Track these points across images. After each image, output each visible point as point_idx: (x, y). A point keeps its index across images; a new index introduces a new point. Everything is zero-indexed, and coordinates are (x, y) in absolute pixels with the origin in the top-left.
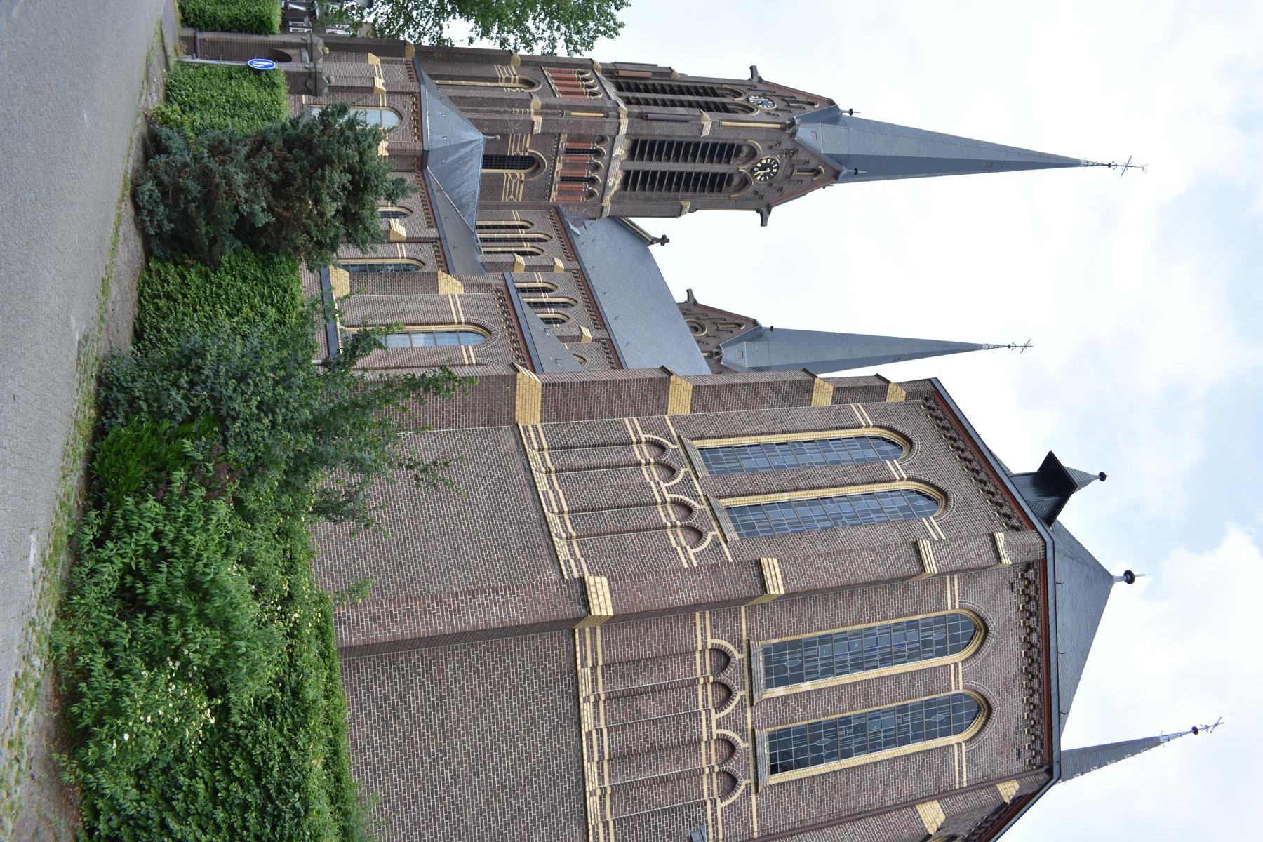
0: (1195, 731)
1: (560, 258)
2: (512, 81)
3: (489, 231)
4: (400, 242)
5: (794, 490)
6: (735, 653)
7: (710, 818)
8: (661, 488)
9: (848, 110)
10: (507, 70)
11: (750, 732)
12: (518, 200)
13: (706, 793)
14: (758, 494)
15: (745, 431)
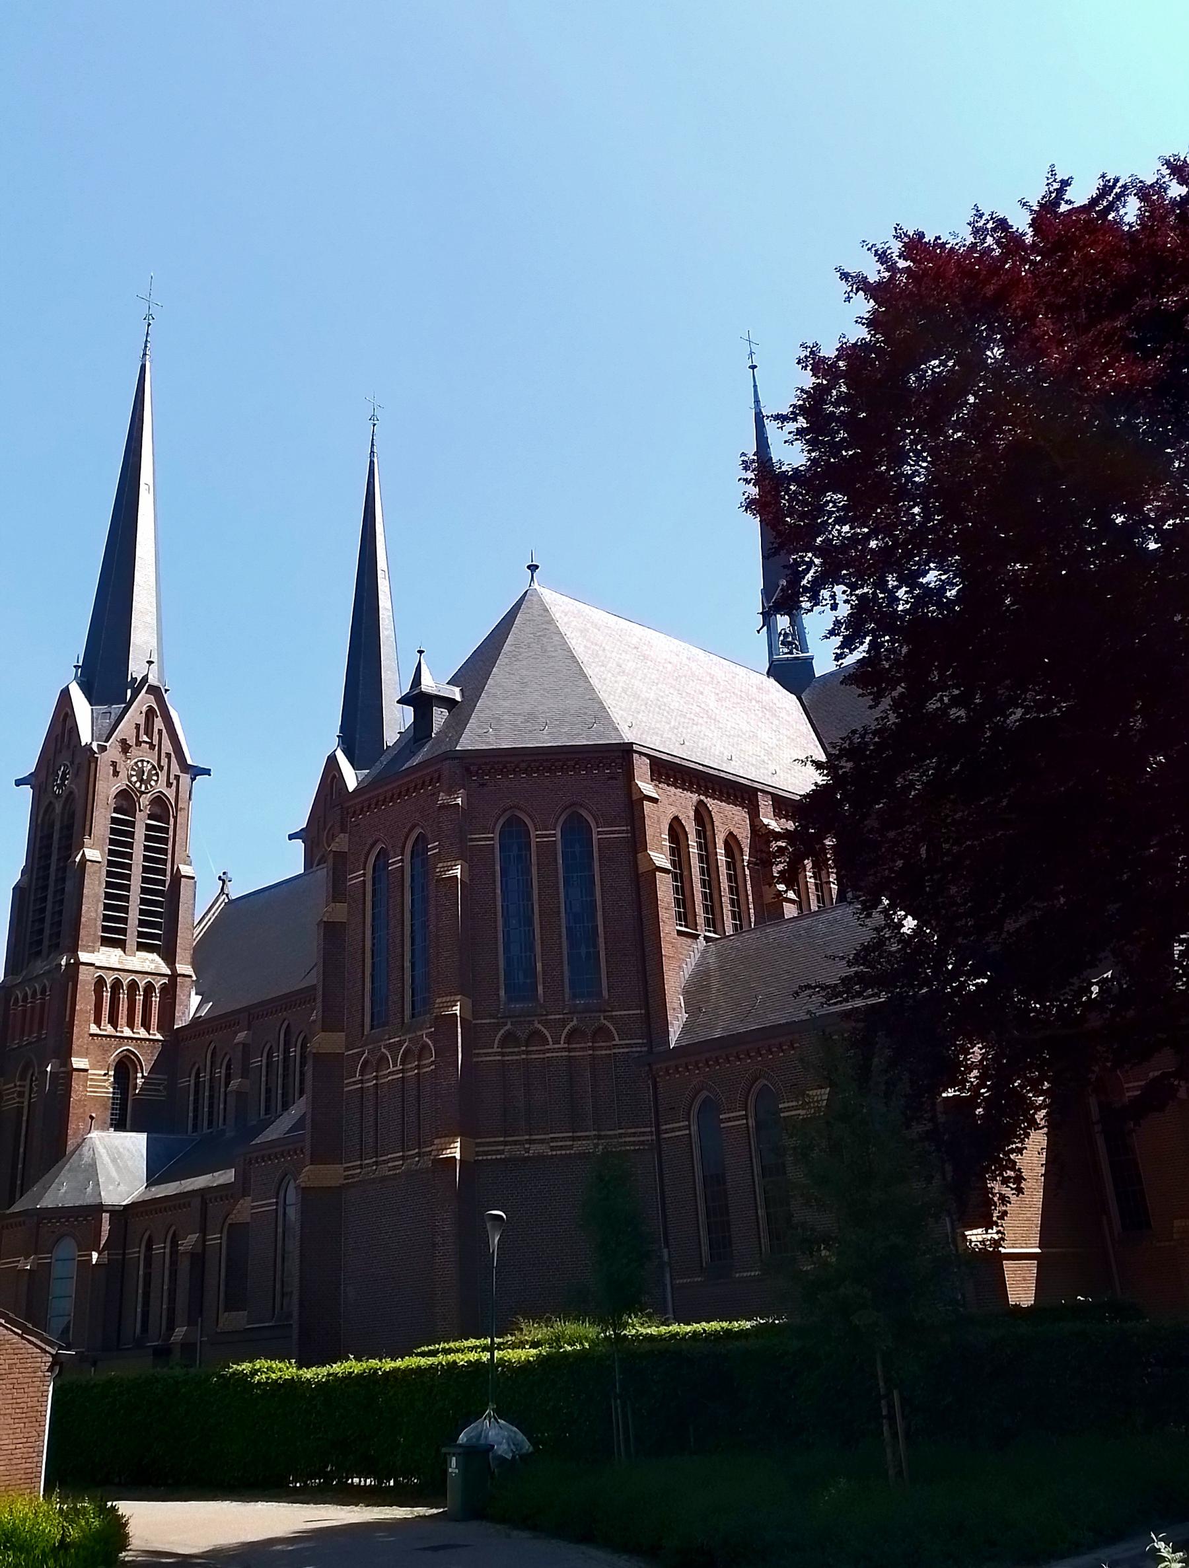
0: (753, 367)
1: (236, 1033)
2: (22, 1089)
3: (200, 1118)
4: (204, 1241)
5: (403, 958)
6: (506, 1028)
7: (626, 1050)
8: (393, 1071)
9: (75, 669)
10: (8, 1094)
11: (566, 1016)
12: (165, 1080)
13: (608, 1052)
14: (403, 990)
15: (360, 988)
